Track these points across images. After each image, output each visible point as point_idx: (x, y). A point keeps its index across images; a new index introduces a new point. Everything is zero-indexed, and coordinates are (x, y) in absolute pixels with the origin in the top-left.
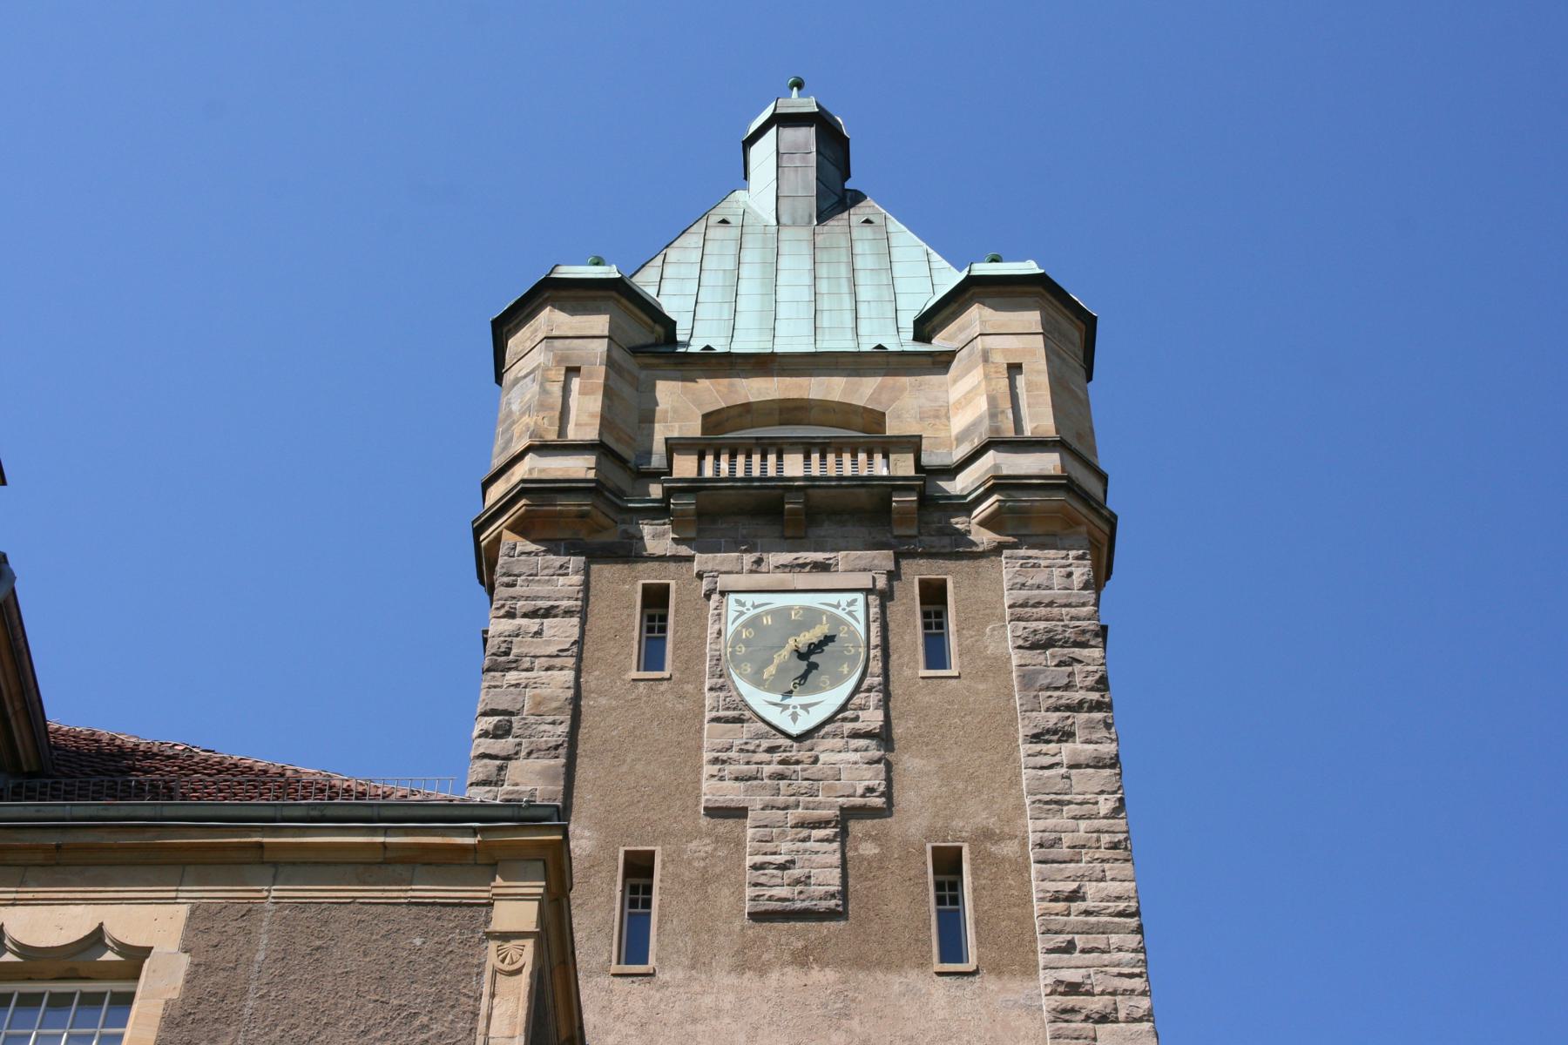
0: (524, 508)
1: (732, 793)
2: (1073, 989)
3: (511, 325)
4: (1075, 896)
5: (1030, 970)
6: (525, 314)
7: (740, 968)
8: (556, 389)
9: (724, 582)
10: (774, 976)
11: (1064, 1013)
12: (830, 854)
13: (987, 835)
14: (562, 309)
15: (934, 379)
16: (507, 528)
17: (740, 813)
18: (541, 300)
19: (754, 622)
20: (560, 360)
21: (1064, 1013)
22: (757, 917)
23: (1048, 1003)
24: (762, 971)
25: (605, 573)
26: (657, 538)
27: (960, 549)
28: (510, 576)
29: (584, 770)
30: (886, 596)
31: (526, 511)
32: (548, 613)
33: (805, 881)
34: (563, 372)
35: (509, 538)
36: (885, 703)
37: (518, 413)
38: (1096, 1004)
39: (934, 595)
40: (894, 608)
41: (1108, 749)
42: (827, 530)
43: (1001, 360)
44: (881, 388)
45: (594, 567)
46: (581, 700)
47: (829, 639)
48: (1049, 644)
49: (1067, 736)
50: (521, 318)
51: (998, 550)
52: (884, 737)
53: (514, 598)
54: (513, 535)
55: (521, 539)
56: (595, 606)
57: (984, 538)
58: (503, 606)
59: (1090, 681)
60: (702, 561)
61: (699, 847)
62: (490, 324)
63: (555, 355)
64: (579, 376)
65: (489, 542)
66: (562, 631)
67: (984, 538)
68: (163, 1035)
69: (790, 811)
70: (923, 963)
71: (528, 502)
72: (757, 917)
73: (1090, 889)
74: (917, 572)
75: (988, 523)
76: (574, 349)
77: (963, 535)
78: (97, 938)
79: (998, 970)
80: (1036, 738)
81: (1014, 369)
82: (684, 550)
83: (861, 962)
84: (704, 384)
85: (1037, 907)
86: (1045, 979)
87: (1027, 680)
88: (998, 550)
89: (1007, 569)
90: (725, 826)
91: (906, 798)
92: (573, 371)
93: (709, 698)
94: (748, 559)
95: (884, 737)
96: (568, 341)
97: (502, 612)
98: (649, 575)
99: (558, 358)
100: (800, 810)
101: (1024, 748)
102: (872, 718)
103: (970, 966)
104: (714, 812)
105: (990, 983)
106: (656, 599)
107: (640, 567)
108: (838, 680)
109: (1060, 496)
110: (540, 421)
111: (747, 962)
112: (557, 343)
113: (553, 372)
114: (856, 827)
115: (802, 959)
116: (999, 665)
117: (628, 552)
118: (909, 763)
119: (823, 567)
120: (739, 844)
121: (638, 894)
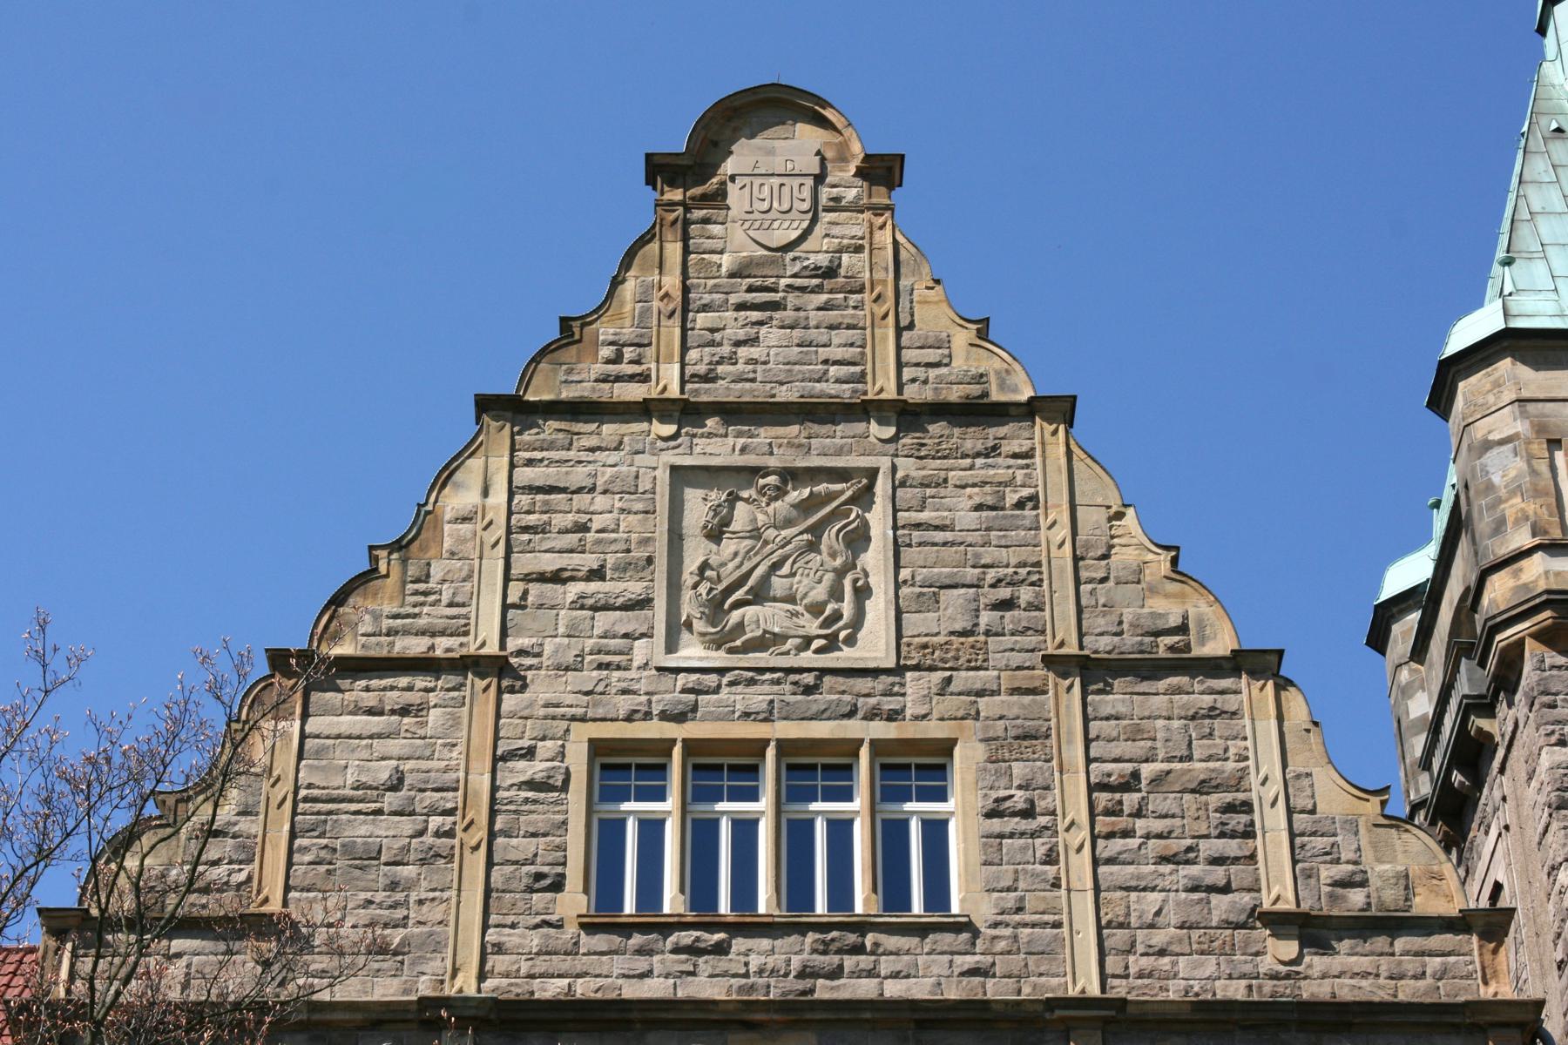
0: (1550, 620)
3: (1461, 367)
6: (1480, 357)
8: (1543, 467)
14: (1524, 362)
16: (1530, 635)
18: (1498, 348)
20: (1540, 428)
28: (1548, 694)
31: (1554, 624)
34: (1545, 446)
35: (1531, 646)
37: (1504, 491)
45: (873, 188)
46: (689, 304)
50: (1473, 361)
53: (1560, 722)
54: (1537, 644)
55: (1547, 649)
58: (1553, 732)
59: (1226, 976)
62: (1435, 367)
63: (1531, 422)
64: (1561, 449)
65: (1508, 645)
69: (1004, 841)
71: (1555, 615)
76: (1548, 416)
96: (1540, 405)
97: (1553, 739)
99: (1536, 428)
100: (676, 694)
110: (1539, 511)
112: (1531, 407)
113: (1536, 446)
121: (822, 780)
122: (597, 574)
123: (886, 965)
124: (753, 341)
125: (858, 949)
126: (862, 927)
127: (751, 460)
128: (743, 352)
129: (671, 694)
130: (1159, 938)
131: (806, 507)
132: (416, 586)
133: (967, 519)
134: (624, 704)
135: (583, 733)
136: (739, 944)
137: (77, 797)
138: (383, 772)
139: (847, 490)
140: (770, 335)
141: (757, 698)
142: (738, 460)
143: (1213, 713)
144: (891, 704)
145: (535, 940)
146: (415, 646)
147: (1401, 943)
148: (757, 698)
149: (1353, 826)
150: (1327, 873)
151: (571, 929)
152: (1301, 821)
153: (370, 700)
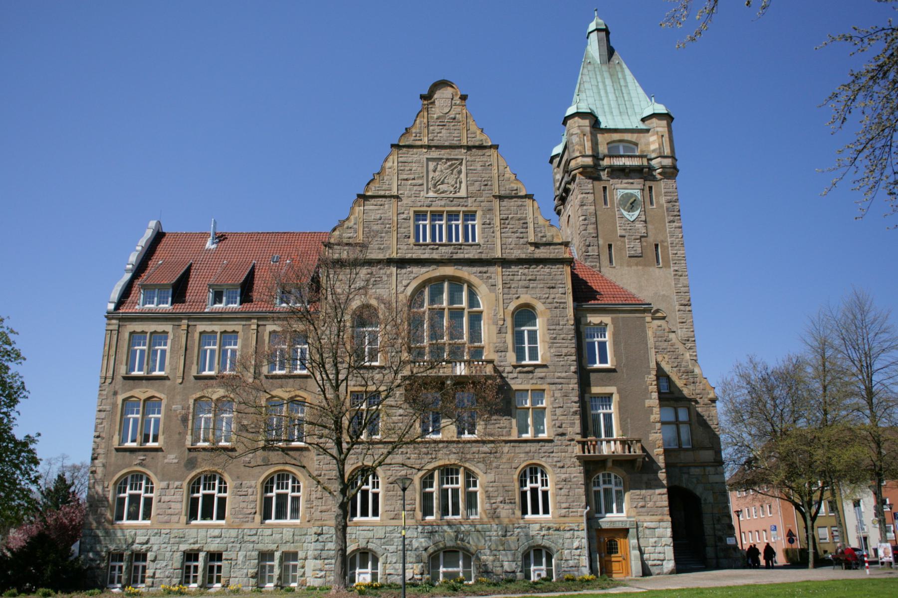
1: (623, 233)
2: (677, 271)
4: (676, 254)
5: (670, 267)
7: (628, 266)
9: (617, 186)
10: (633, 268)
11: (675, 275)
12: (639, 245)
13: (662, 241)
15: (646, 135)
17: (624, 236)
19: (622, 196)
21: (675, 275)
22: (629, 257)
23: (673, 273)
24: (631, 266)
25: (596, 183)
26: (604, 175)
27: (654, 179)
29: (599, 227)
30: (643, 190)
32: (588, 193)
33: (636, 250)
35: (578, 175)
36: (645, 215)
38: (680, 273)
39: (651, 188)
40: (645, 192)
41: (680, 224)
42: (632, 174)
43: (660, 134)
44: (637, 137)
47: (635, 200)
48: (670, 202)
49: (674, 222)
51: (661, 179)
52: (645, 222)
56: (596, 192)
57: (659, 177)
60: (611, 181)
61: (619, 243)
66: (591, 197)
67: (659, 177)
68: (844, 567)
70: (654, 266)
72: (629, 257)
73: (679, 252)
74: (648, 184)
75: (660, 174)
77: (654, 176)
78: (601, 322)
79: (665, 267)
80: (669, 222)
81: (662, 136)
82: (609, 179)
83: (645, 265)
84: (606, 135)
85: (671, 256)
86: (672, 269)
87: (667, 209)
88: (661, 179)
89: (662, 184)
90: (622, 239)
91: (650, 234)
92: (584, 135)
93: (617, 213)
94: (620, 181)
95: (645, 222)
98: (603, 184)
101: (667, 224)
102: (643, 218)
103: (661, 266)
104: (621, 236)
105: (664, 269)
106: (605, 188)
107: (602, 182)
108: (637, 209)
109: (672, 170)
111: (629, 265)
114: (643, 239)
115: (637, 265)
116: (662, 206)
117: (598, 179)
118: (650, 226)
119: (632, 183)
120: (625, 243)
122: (414, 179)
123: (465, 251)
124: (440, 133)
125: (460, 249)
126: (461, 245)
127: (441, 156)
128: (439, 135)
129: (428, 202)
130: (511, 247)
131: (451, 166)
132: (559, 374)
133: (479, 168)
134: (419, 204)
135: (413, 209)
136: (440, 248)
137: (378, 542)
138: (378, 217)
139: (458, 162)
140: (444, 131)
141: (443, 203)
142: (438, 157)
143: (522, 206)
144: (466, 204)
145: (406, 247)
146: (382, 193)
147: (551, 247)
148: (443, 203)
149: (544, 226)
150: (540, 235)
151: (412, 245)
152: (536, 225)
153: (375, 203)
